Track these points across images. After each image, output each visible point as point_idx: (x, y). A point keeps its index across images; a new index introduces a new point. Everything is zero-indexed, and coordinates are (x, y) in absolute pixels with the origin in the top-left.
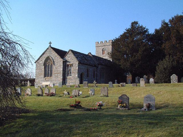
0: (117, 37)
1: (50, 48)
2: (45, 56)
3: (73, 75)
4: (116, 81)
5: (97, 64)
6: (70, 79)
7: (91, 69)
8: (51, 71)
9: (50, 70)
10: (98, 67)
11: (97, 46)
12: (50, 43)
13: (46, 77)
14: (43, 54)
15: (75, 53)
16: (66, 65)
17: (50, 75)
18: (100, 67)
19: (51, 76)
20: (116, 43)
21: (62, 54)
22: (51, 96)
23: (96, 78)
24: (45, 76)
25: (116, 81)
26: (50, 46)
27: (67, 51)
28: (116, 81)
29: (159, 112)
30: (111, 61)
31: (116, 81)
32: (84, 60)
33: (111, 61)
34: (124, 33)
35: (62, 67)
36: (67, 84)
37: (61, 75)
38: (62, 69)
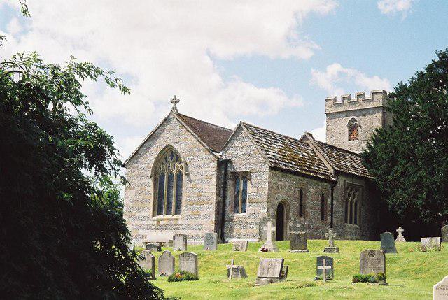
0: (406, 81)
1: (175, 124)
2: (159, 145)
3: (250, 208)
4: (400, 230)
5: (332, 171)
6: (242, 221)
7: (313, 190)
8: (179, 195)
9: (174, 191)
10: (334, 184)
11: (331, 110)
12: (175, 101)
13: (159, 213)
14: (153, 137)
15: (263, 136)
16: (230, 181)
17: (164, 211)
18: (341, 181)
19: (178, 211)
20: (397, 103)
21: (213, 137)
22: (170, 280)
23: (329, 219)
24: (158, 210)
25: (402, 230)
26: (175, 109)
27: (232, 126)
28: (402, 230)
29: (259, 86)
30: (313, 70)
31: (400, 230)
32: (293, 162)
33: (313, 70)
34: (431, 63)
35: (214, 180)
36: (230, 240)
37: (213, 208)
38: (213, 189)
